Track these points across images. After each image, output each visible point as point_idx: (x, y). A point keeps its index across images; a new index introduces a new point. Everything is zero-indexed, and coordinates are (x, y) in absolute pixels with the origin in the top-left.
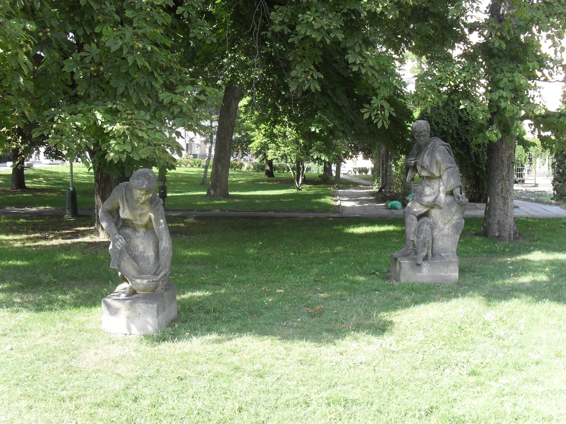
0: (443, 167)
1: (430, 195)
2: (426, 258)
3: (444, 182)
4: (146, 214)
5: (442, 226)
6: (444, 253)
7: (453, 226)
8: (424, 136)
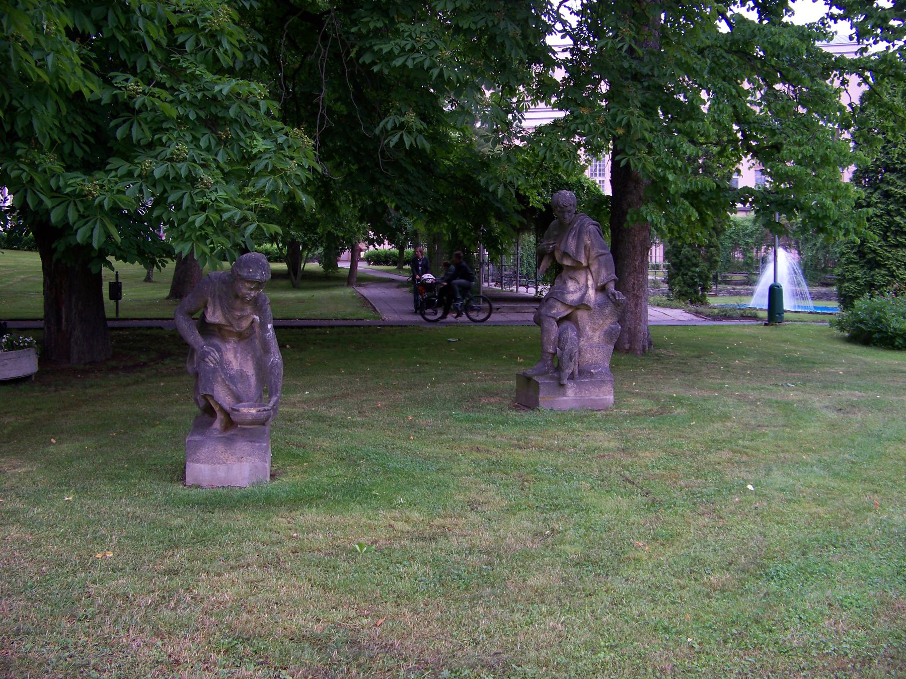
0: (593, 254)
1: (575, 292)
2: (572, 377)
3: (594, 275)
4: (248, 316)
5: (590, 333)
6: (594, 368)
8: (569, 212)
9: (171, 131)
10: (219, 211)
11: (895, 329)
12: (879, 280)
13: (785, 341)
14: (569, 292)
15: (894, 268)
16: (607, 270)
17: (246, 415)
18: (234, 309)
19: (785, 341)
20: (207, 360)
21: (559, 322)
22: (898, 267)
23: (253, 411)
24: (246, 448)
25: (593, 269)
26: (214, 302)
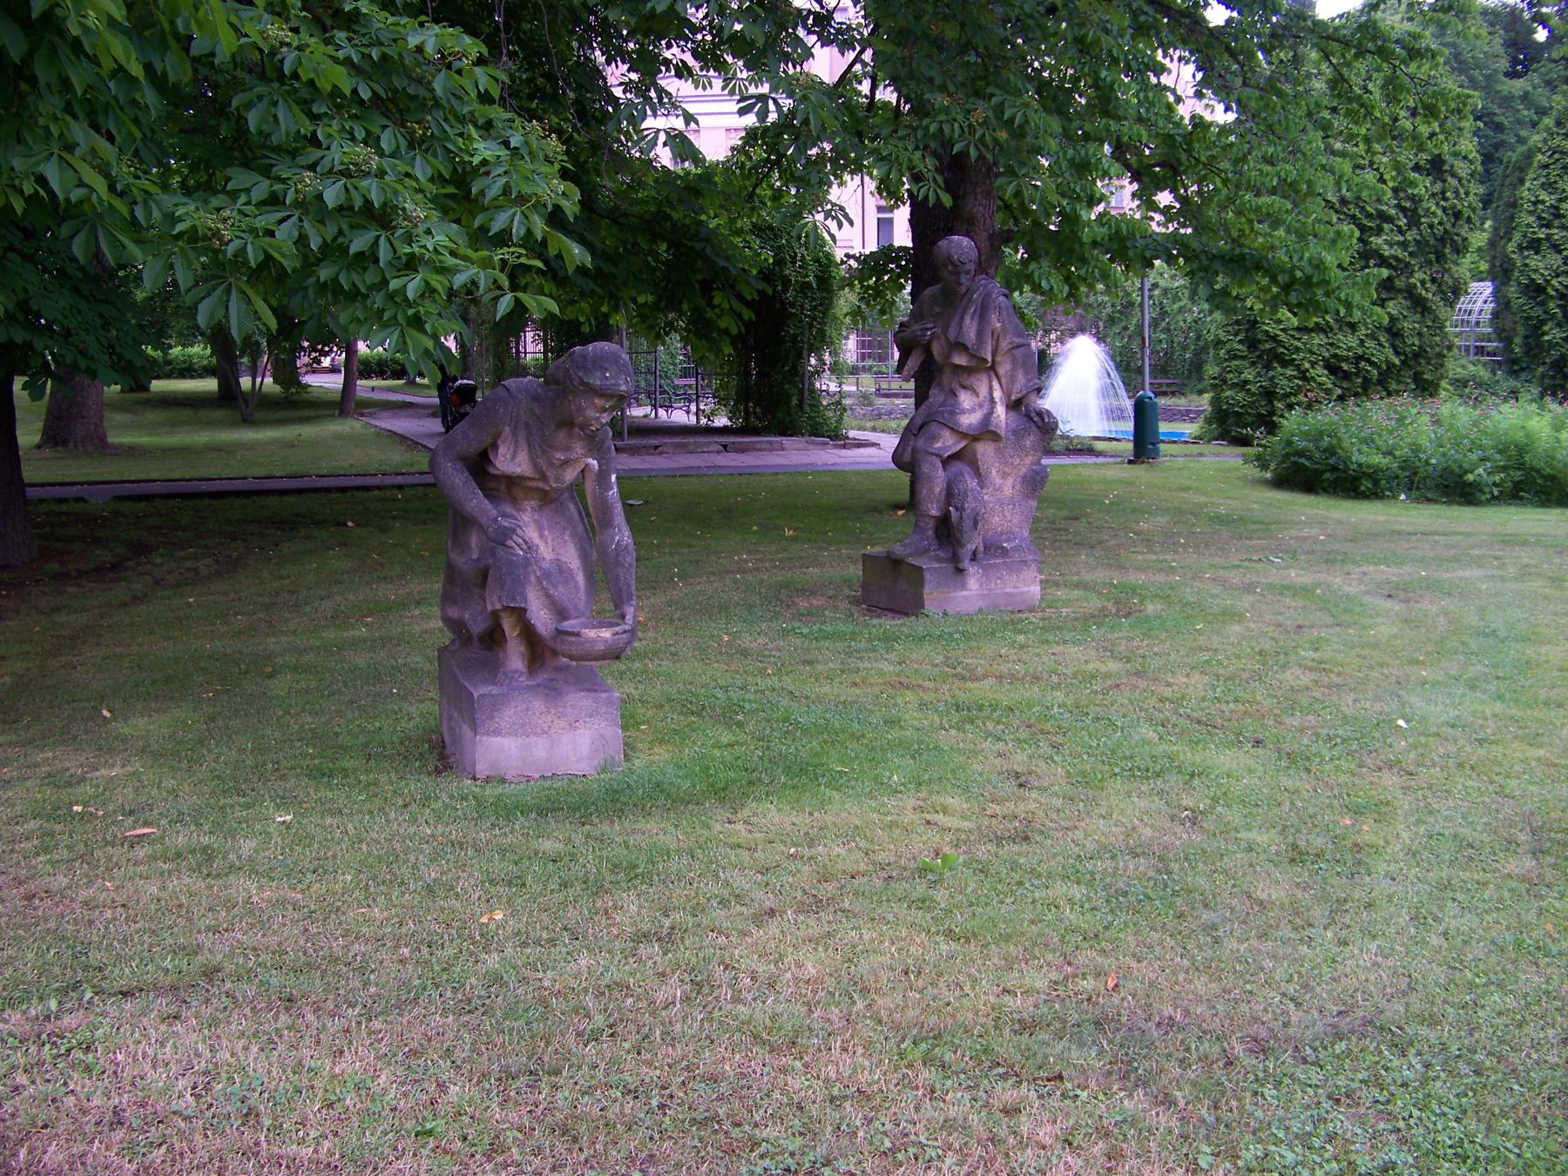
1: (973, 410)
2: (974, 557)
3: (1004, 381)
4: (576, 460)
5: (998, 481)
6: (1007, 541)
7: (1024, 477)
9: (325, 120)
10: (442, 270)
11: (1360, 465)
12: (1283, 385)
13: (1186, 489)
14: (963, 412)
15: (1307, 365)
16: (1026, 373)
17: (594, 641)
18: (551, 446)
19: (1186, 489)
20: (510, 543)
21: (946, 462)
22: (1313, 364)
23: (606, 634)
24: (585, 703)
25: (1001, 371)
26: (515, 436)
